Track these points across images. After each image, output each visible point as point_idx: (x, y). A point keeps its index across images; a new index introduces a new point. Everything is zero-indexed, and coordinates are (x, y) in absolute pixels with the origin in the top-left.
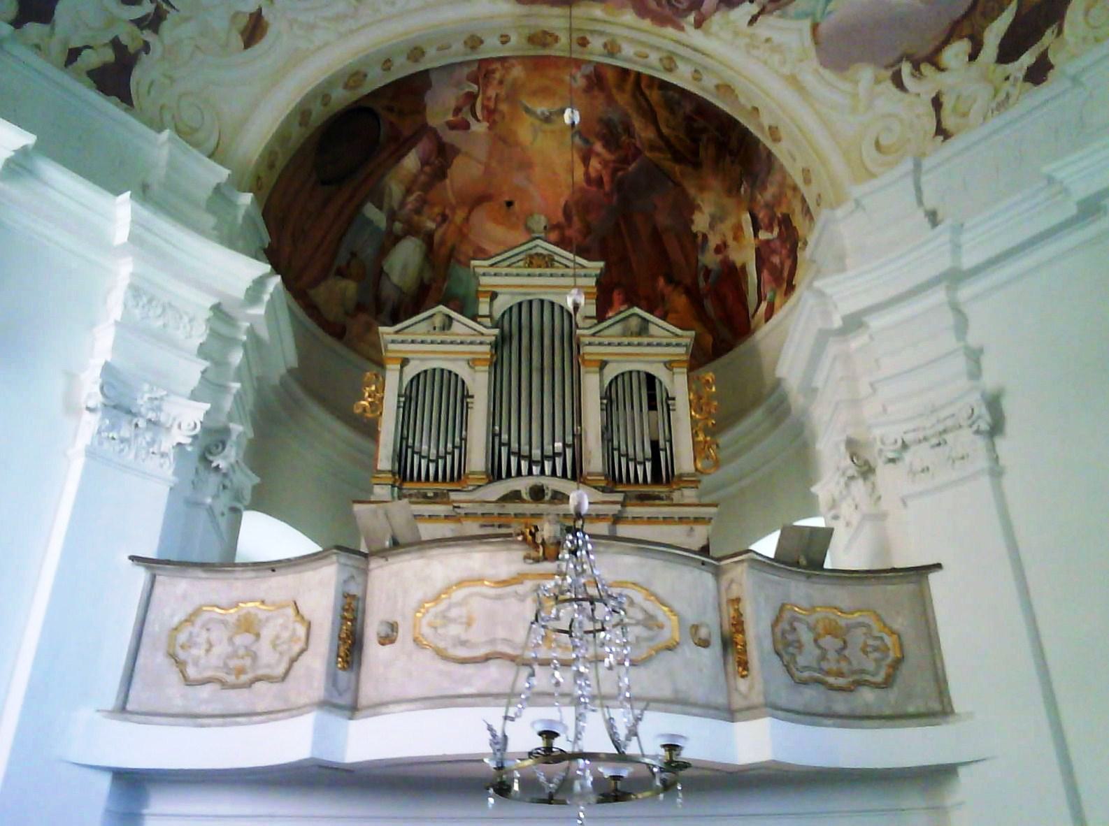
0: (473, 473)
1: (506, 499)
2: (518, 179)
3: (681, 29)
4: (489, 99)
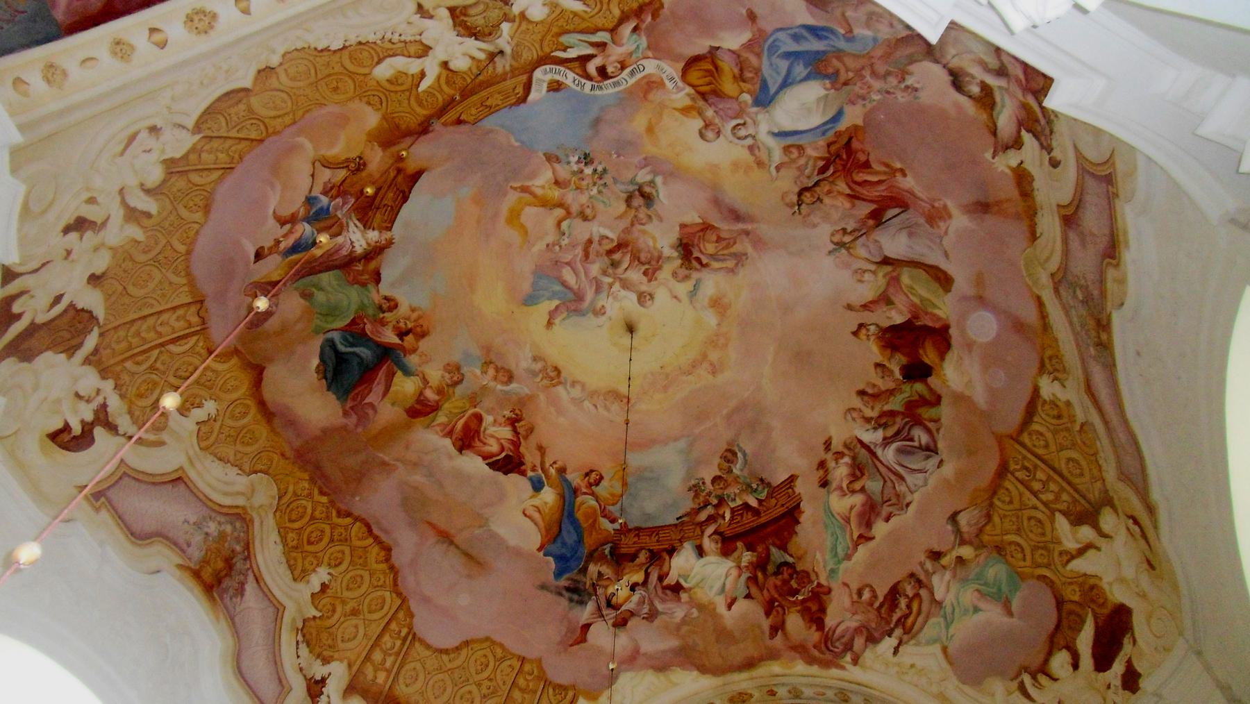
3: (843, 668)
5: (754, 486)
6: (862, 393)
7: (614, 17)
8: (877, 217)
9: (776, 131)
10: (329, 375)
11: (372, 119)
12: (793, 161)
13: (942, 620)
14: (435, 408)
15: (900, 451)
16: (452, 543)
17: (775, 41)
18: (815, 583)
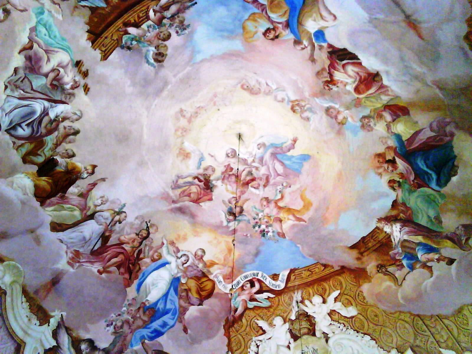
5: (134, 43)
6: (76, 133)
7: (245, 317)
8: (105, 238)
9: (167, 265)
10: (450, 164)
11: (366, 287)
12: (156, 251)
14: (387, 107)
15: (33, 113)
16: (408, 17)
17: (174, 318)
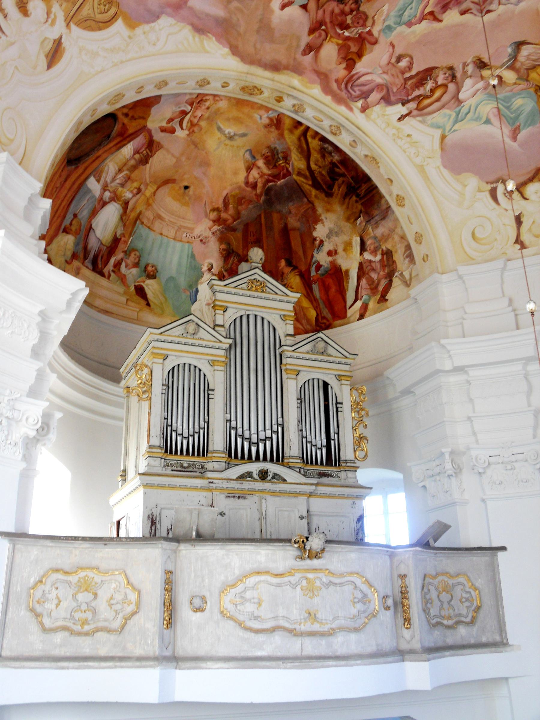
0: (214, 452)
1: (242, 477)
2: (197, 172)
3: (351, 109)
4: (195, 117)
13: (454, 115)
18: (367, 29)
